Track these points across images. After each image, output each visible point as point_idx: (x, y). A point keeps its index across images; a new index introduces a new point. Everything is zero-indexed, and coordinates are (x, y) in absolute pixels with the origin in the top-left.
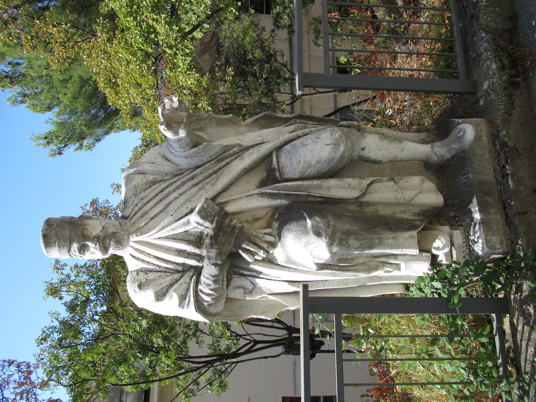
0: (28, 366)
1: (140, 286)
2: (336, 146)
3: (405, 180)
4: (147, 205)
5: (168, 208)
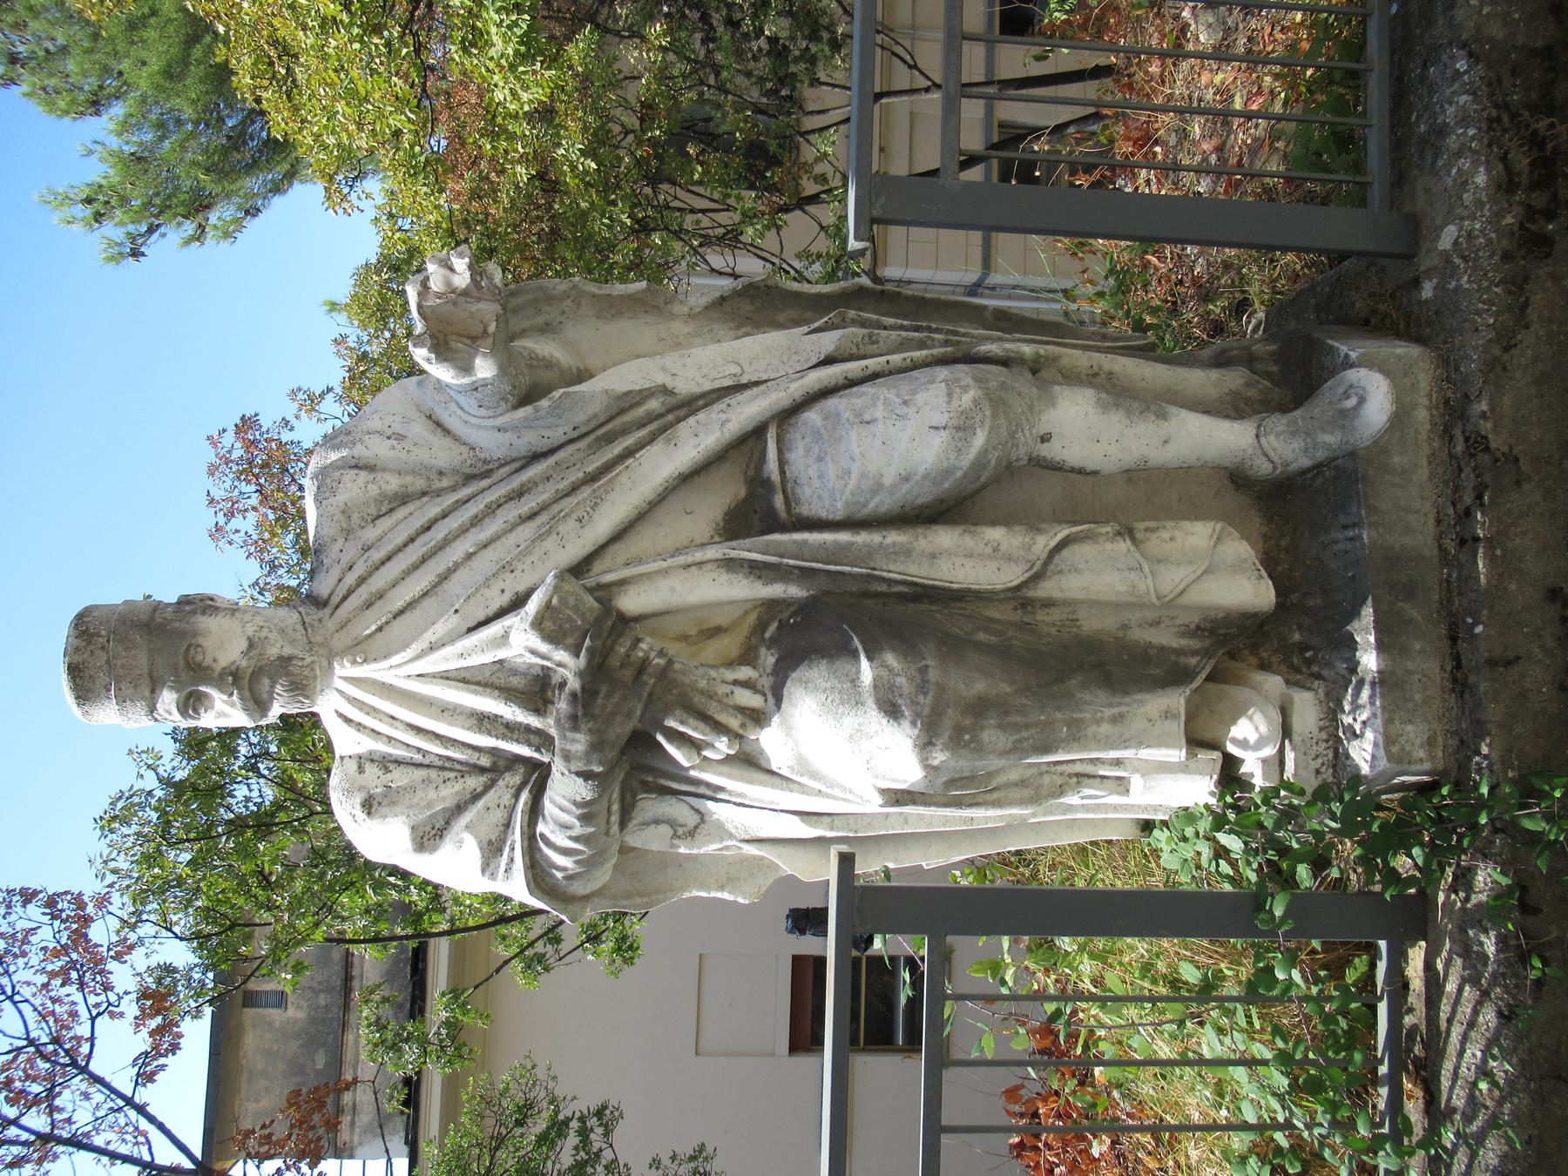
0: (79, 902)
1: (369, 806)
2: (961, 434)
3: (1166, 535)
4: (384, 569)
5: (446, 586)
